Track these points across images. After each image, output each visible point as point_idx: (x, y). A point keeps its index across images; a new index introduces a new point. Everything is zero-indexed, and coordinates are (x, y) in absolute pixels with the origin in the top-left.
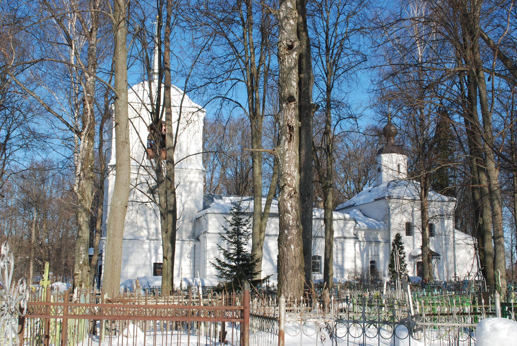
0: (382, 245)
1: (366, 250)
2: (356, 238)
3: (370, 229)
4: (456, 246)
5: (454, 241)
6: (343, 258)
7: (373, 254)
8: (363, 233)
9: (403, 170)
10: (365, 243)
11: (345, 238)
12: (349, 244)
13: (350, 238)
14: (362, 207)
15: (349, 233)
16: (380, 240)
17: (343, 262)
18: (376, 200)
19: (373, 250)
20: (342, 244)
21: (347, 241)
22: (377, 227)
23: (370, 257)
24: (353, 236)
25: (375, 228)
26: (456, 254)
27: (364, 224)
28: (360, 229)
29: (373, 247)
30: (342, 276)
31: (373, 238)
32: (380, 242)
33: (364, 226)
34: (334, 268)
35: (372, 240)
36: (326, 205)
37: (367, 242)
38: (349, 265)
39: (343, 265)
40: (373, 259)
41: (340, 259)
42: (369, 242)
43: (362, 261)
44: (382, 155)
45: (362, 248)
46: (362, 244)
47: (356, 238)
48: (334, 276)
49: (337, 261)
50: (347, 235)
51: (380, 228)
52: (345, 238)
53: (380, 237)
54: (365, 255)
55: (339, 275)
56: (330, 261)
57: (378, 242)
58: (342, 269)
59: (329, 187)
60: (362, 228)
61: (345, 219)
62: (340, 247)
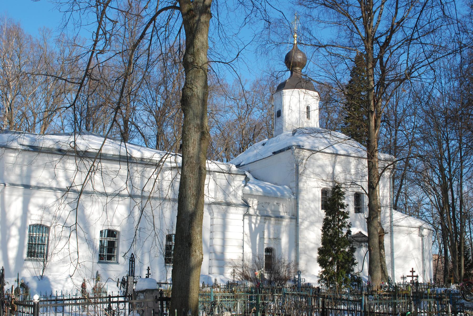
0: (285, 222)
1: (260, 230)
2: (246, 205)
3: (267, 196)
4: (394, 228)
5: (391, 222)
6: (224, 240)
7: (272, 237)
8: (256, 202)
9: (315, 115)
10: (259, 218)
11: (229, 204)
12: (236, 216)
13: (237, 205)
14: (251, 167)
15: (235, 196)
16: (282, 214)
17: (223, 246)
18: (275, 153)
19: (272, 231)
20: (224, 216)
21: (232, 210)
22: (279, 194)
23: (266, 241)
24: (240, 201)
25: (275, 193)
26: (395, 241)
27: (257, 187)
28: (251, 195)
29: (271, 226)
30: (222, 273)
31: (272, 211)
32: (282, 217)
33: (257, 191)
34: (206, 259)
35: (270, 213)
36: (190, 59)
37: (262, 216)
38: (233, 254)
39: (223, 253)
40: (272, 246)
41: (217, 242)
42: (266, 217)
43: (253, 248)
44: (284, 91)
45: (253, 226)
46: (254, 220)
47: (246, 205)
48: (204, 268)
49: (212, 245)
50: (232, 199)
51: (283, 195)
52: (229, 204)
53: (282, 211)
54: (258, 238)
55: (215, 270)
56: (195, 224)
57: (279, 218)
58: (221, 261)
59: (202, 13)
60: (255, 193)
61: (229, 172)
62: (218, 221)
